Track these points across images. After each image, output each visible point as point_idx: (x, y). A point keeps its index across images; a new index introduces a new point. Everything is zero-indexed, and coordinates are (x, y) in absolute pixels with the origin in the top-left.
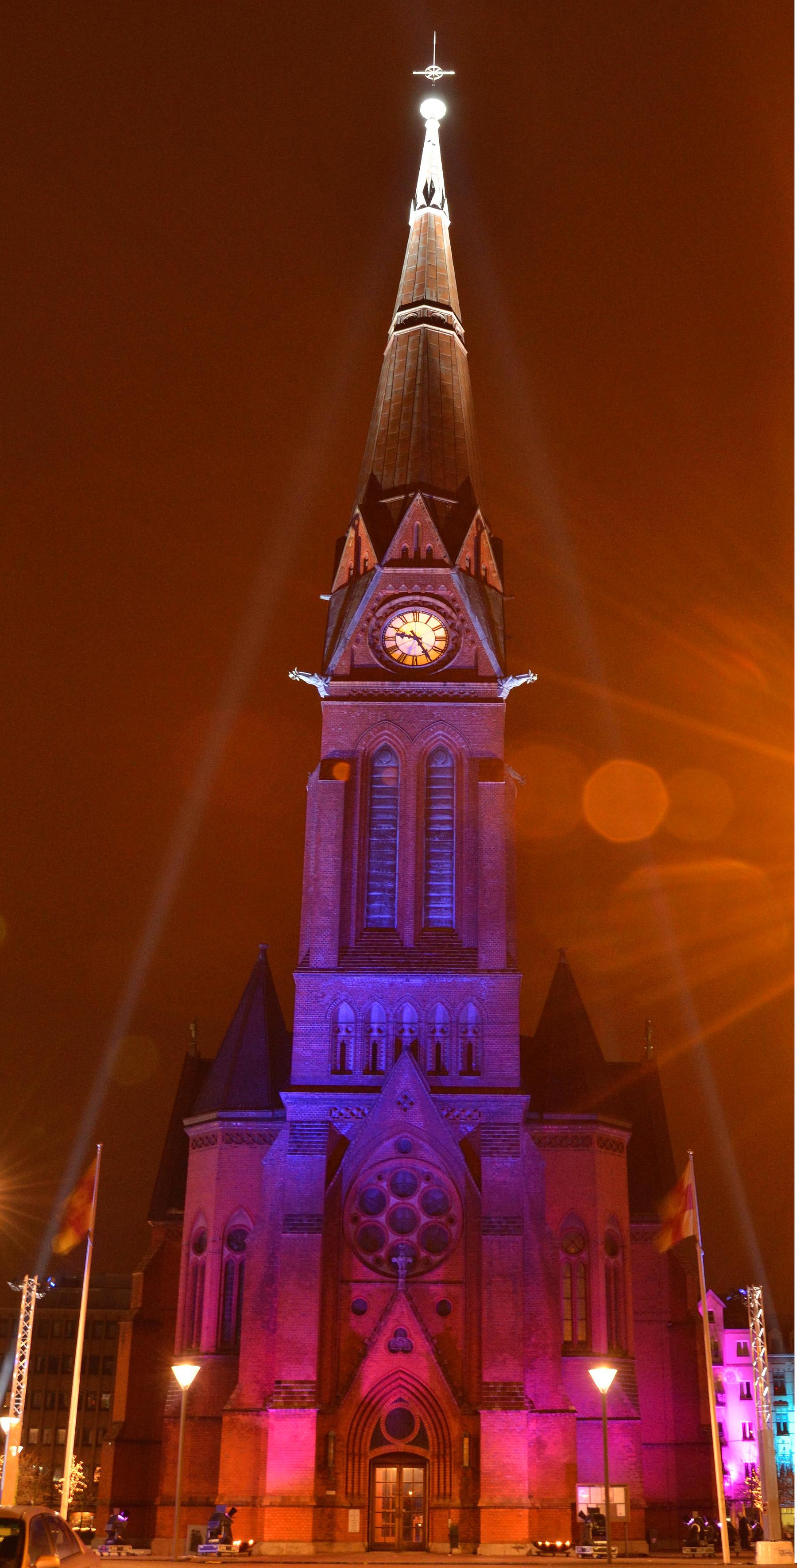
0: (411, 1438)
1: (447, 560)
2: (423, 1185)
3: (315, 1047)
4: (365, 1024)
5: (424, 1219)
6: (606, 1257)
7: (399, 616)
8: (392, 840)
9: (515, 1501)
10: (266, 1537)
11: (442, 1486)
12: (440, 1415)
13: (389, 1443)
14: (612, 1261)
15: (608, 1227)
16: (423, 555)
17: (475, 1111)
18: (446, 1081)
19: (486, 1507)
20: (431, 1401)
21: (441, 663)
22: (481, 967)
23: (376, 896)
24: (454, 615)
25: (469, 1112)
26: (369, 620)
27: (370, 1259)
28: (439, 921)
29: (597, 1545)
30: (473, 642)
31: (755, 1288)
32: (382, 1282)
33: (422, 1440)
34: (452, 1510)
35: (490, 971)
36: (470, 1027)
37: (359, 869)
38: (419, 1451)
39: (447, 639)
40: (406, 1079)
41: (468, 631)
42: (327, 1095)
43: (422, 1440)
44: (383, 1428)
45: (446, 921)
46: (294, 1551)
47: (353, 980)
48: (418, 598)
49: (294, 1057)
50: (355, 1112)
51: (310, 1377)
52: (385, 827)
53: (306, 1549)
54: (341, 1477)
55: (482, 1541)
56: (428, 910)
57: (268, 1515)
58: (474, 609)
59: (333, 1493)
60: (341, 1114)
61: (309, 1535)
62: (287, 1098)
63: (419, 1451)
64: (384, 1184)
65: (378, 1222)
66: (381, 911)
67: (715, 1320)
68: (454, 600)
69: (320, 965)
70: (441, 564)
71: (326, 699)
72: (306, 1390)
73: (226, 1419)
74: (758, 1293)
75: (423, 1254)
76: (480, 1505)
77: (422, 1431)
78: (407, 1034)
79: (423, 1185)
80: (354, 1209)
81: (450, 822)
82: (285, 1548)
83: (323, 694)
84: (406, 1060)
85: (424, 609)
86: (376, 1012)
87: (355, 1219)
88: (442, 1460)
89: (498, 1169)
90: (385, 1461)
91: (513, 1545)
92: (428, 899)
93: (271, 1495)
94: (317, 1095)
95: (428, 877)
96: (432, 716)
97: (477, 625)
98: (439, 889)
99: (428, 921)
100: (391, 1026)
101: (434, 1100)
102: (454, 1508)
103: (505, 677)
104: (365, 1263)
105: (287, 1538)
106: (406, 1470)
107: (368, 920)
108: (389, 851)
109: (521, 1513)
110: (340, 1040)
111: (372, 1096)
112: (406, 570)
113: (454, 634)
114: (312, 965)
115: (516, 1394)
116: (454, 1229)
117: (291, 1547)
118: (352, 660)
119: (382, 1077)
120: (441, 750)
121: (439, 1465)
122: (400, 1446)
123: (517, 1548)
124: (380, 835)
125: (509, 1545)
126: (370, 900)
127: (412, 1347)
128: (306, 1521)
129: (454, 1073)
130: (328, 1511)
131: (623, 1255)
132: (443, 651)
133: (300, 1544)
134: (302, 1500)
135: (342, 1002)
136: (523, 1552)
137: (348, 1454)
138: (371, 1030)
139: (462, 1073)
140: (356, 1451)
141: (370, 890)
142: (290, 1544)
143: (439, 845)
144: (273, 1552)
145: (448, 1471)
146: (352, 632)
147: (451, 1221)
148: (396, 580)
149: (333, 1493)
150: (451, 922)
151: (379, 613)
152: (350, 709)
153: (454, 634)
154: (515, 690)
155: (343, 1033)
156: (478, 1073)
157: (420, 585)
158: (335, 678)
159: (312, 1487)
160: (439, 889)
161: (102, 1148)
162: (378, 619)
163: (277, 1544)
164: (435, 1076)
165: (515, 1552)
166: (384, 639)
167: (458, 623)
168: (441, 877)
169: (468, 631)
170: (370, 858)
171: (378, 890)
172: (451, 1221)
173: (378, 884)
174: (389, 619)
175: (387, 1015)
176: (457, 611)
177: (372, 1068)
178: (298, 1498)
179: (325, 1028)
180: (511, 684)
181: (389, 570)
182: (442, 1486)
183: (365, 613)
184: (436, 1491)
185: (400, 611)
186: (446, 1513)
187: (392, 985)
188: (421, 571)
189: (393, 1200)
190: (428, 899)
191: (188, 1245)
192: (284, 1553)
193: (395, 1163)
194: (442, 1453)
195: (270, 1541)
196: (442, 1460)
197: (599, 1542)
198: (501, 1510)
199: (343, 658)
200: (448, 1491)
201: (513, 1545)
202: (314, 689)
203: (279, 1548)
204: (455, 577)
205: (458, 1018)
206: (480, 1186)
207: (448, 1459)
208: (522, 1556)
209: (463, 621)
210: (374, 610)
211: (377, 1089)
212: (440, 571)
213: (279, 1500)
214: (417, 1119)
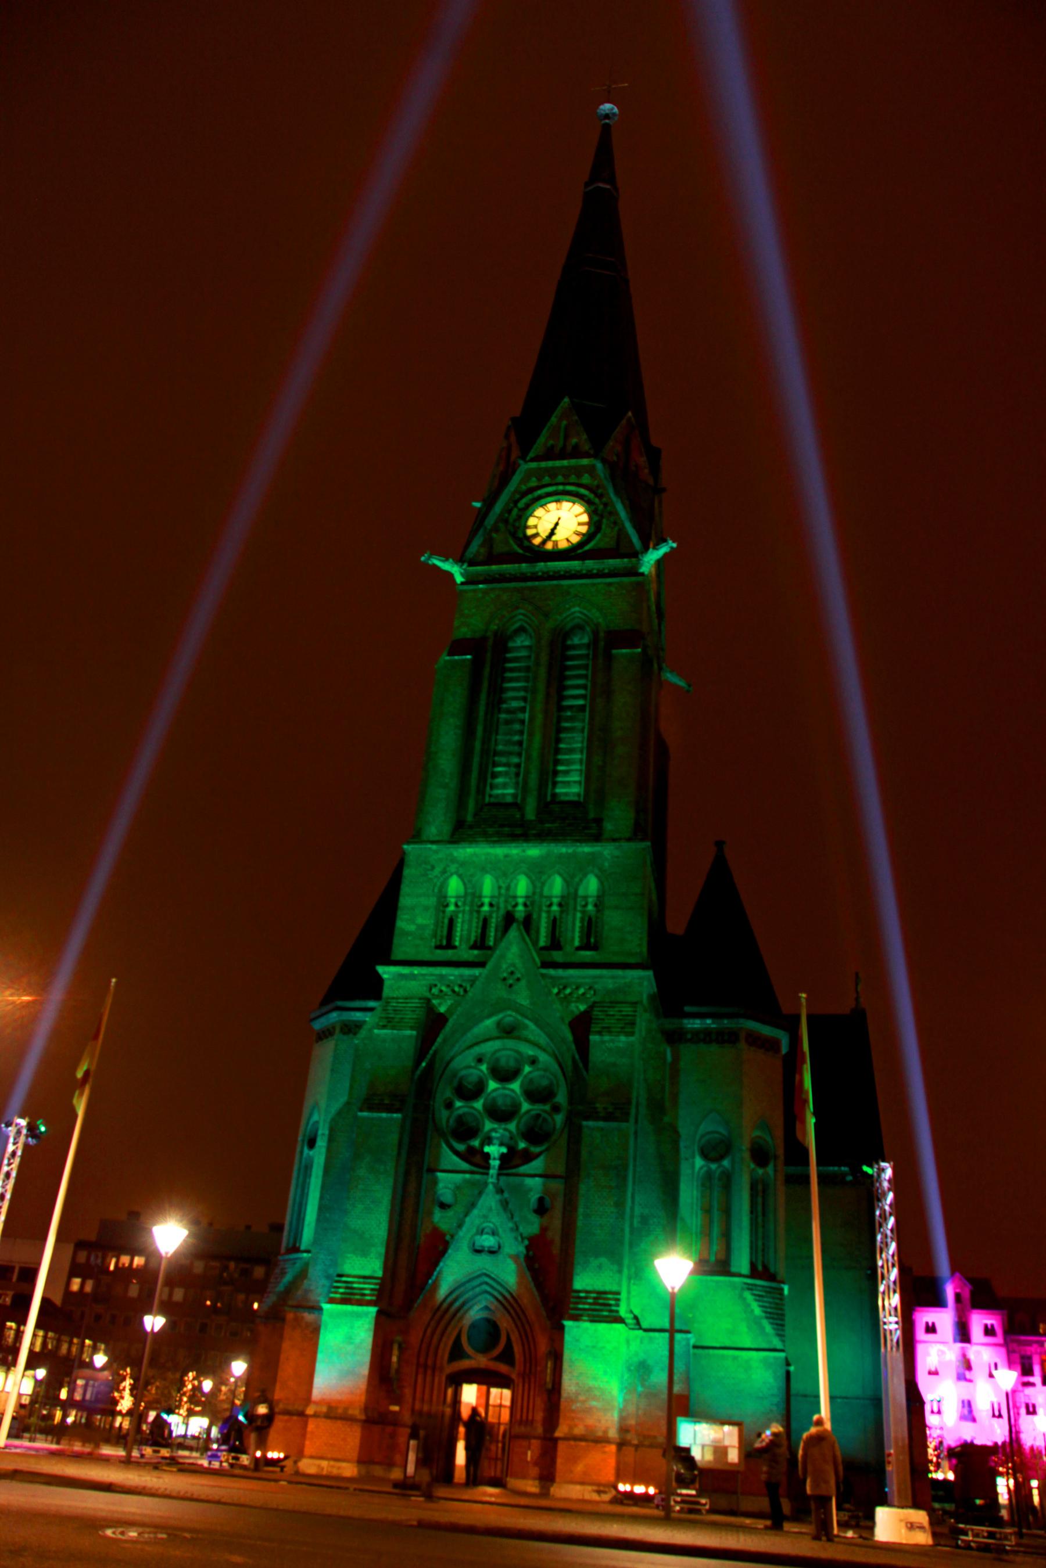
0: (496, 1352)
1: (592, 452)
2: (527, 1069)
3: (420, 921)
4: (473, 896)
5: (526, 1106)
6: (752, 1166)
7: (542, 506)
8: (520, 716)
9: (600, 1434)
10: (308, 1451)
11: (525, 1410)
12: (527, 1327)
13: (469, 1357)
14: (760, 1171)
15: (757, 1133)
16: (569, 449)
17: (590, 988)
18: (557, 956)
19: (566, 1439)
20: (518, 1309)
21: (580, 545)
22: (606, 835)
23: (500, 772)
24: (597, 500)
25: (581, 991)
26: (510, 512)
27: (461, 1147)
28: (566, 794)
29: (681, 1495)
30: (615, 523)
31: (883, 1164)
32: (472, 1172)
33: (507, 1356)
34: (533, 1441)
35: (614, 840)
36: (590, 900)
37: (483, 743)
38: (503, 1368)
39: (589, 524)
40: (512, 951)
41: (611, 513)
42: (424, 970)
43: (507, 1356)
44: (464, 1340)
45: (574, 794)
46: (335, 1472)
47: (466, 852)
48: (561, 488)
49: (397, 932)
50: (457, 989)
51: (374, 1271)
52: (515, 704)
53: (349, 1470)
54: (408, 1392)
55: (557, 1479)
56: (555, 784)
57: (311, 1426)
58: (617, 493)
59: (396, 1408)
60: (441, 991)
61: (355, 1455)
62: (385, 973)
63: (503, 1368)
64: (484, 1067)
65: (473, 1108)
66: (505, 786)
67: (481, 959)
68: (598, 487)
69: (432, 838)
70: (587, 455)
71: (462, 583)
72: (368, 1287)
73: (290, 1316)
74: (888, 1173)
75: (522, 1145)
76: (557, 1434)
77: (509, 1345)
78: (520, 908)
79: (527, 1069)
80: (448, 1093)
81: (583, 697)
82: (325, 1466)
83: (459, 579)
84: (513, 933)
85: (568, 497)
86: (488, 886)
87: (449, 1105)
88: (527, 1380)
89: (609, 1047)
90: (471, 1376)
91: (595, 1488)
92: (556, 773)
93: (317, 1403)
94: (416, 970)
95: (557, 751)
96: (568, 593)
97: (620, 507)
98: (568, 762)
99: (554, 795)
100: (502, 900)
101: (543, 976)
102: (535, 1438)
103: (646, 549)
104: (456, 1153)
105: (329, 1456)
106: (494, 1391)
107: (490, 796)
108: (517, 727)
109: (607, 1449)
110: (448, 915)
111: (476, 971)
112: (550, 464)
113: (596, 518)
114: (424, 838)
115: (610, 1305)
116: (559, 1119)
117: (333, 1467)
118: (491, 547)
119: (489, 952)
120: (580, 627)
121: (523, 1386)
122: (481, 1361)
123: (599, 1492)
124: (509, 711)
125: (590, 1488)
126: (495, 775)
127: (499, 1247)
128: (352, 1438)
129: (568, 949)
130: (389, 1429)
131: (775, 1166)
132: (583, 535)
133: (344, 1464)
134: (350, 1412)
135: (452, 875)
136: (607, 1497)
137: (418, 1365)
138: (482, 905)
139: (578, 949)
140: (430, 1363)
141: (495, 765)
142: (332, 1463)
143: (571, 719)
144: (312, 1470)
145: (532, 1393)
146: (492, 522)
147: (556, 1109)
148: (539, 474)
149: (396, 1408)
150: (579, 795)
151: (521, 505)
152: (485, 592)
153: (596, 518)
154: (658, 562)
155: (452, 908)
156: (595, 948)
157: (564, 476)
158: (471, 563)
159: (363, 1398)
160: (568, 762)
161: (116, 983)
162: (520, 510)
163: (318, 1462)
164: (551, 953)
165: (595, 1497)
166: (526, 527)
167: (601, 507)
168: (571, 751)
169: (611, 513)
170: (497, 734)
171: (504, 765)
172: (556, 1109)
173: (504, 760)
174: (531, 509)
175: (500, 888)
176: (600, 496)
177: (480, 944)
178: (346, 1409)
179: (432, 901)
180: (651, 559)
181: (534, 465)
182: (525, 1410)
183: (507, 504)
184: (518, 1417)
185: (543, 501)
186: (525, 1443)
187: (506, 856)
188: (565, 463)
189: (492, 1085)
190: (556, 773)
191: (303, 1141)
192: (325, 1472)
193: (496, 1044)
194: (527, 1371)
195: (312, 1457)
196: (527, 1380)
197: (684, 1491)
198: (583, 1444)
199: (482, 545)
200: (530, 1418)
201: (595, 1488)
202: (450, 576)
203: (319, 1466)
204: (599, 465)
205: (576, 891)
206: (587, 1070)
207: (533, 1380)
208: (604, 1502)
209: (606, 505)
210: (516, 502)
211: (482, 964)
212: (585, 462)
213: (324, 1409)
214: (523, 998)
